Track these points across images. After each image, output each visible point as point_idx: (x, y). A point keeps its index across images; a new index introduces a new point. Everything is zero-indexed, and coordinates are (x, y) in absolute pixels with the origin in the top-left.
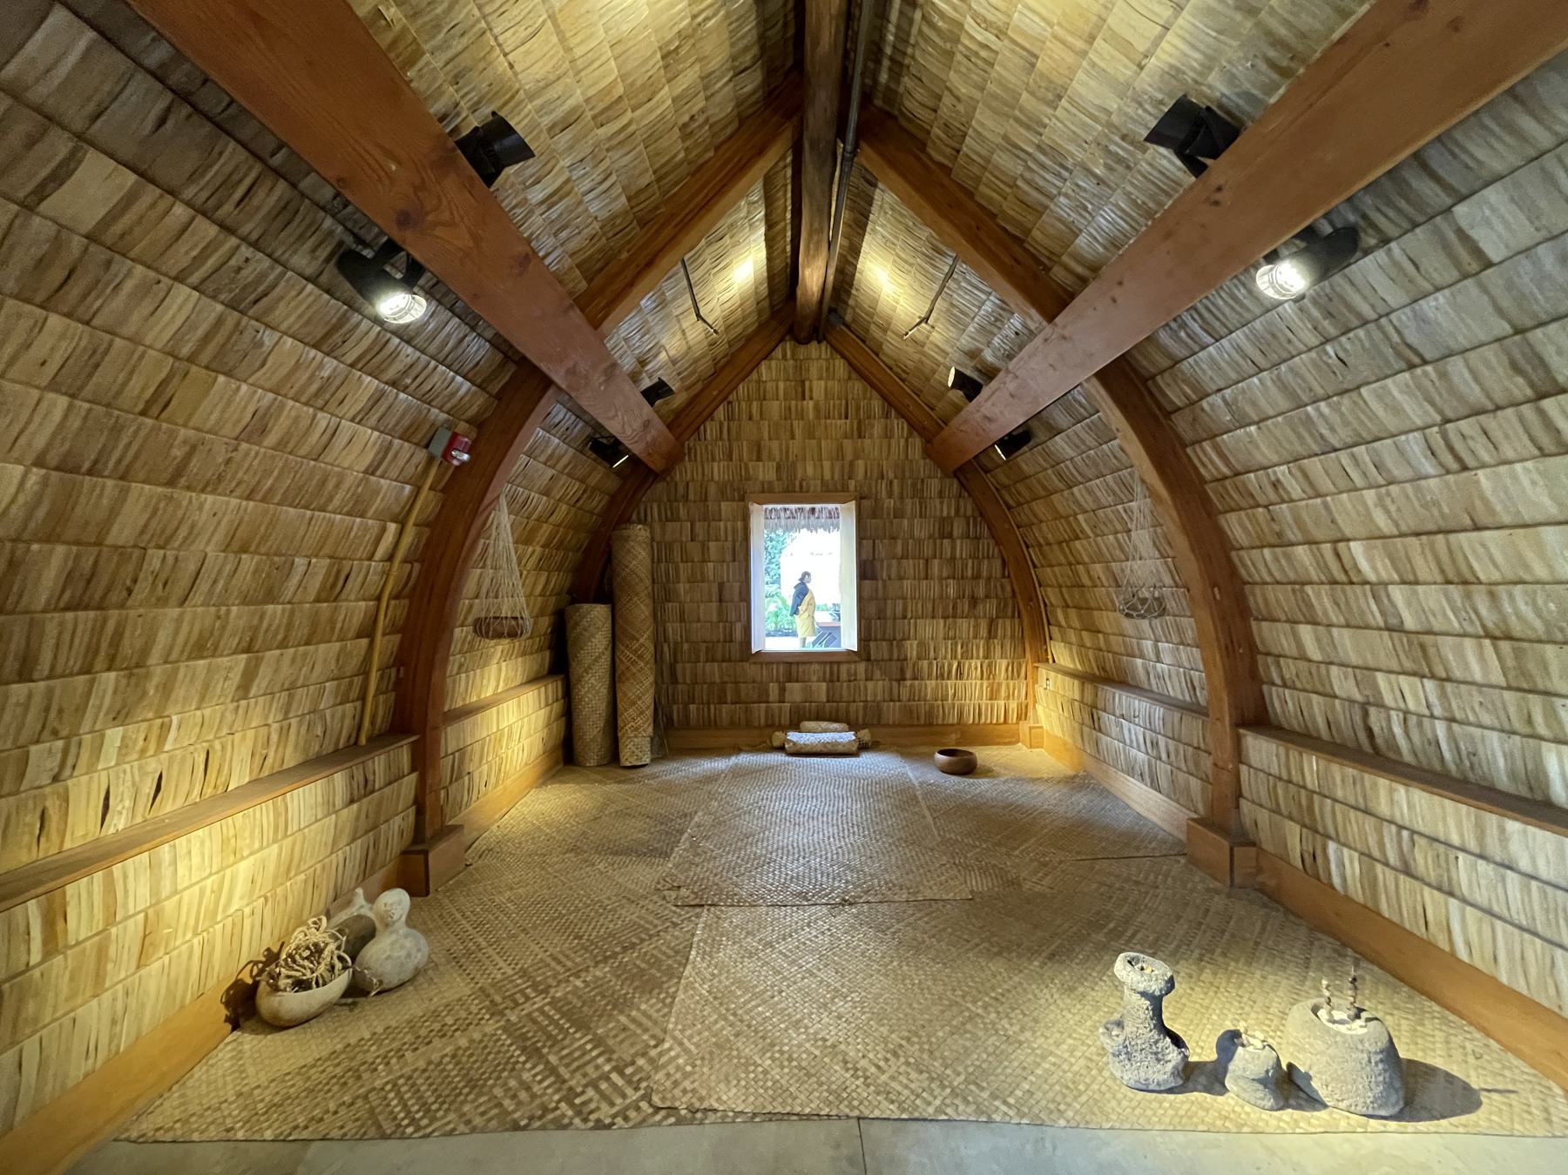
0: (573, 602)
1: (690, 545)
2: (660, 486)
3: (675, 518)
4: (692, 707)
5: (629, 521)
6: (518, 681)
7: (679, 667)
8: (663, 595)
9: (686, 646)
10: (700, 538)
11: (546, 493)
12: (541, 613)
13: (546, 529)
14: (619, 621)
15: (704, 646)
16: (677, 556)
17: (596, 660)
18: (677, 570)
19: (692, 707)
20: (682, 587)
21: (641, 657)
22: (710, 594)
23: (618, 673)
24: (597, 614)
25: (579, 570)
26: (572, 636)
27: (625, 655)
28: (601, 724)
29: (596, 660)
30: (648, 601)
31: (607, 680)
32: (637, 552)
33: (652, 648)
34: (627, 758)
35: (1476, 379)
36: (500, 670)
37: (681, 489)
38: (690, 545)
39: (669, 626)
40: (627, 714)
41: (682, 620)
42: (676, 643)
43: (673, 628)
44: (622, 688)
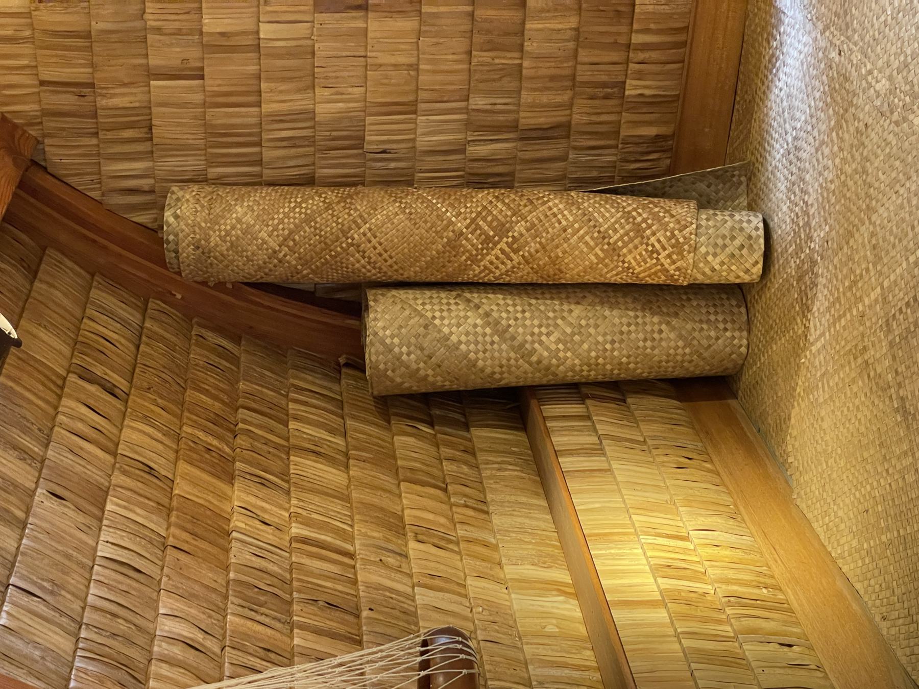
0: (357, 364)
1: (212, 83)
2: (62, 155)
3: (143, 123)
4: (632, 89)
5: (155, 232)
6: (542, 521)
7: (527, 119)
8: (348, 163)
9: (478, 102)
10: (193, 54)
11: (94, 499)
12: (386, 459)
13: (190, 483)
14: (410, 274)
15: (479, 57)
16: (246, 116)
17: (502, 333)
18: (280, 118)
19: (632, 89)
20: (327, 107)
21: (502, 229)
22: (351, 34)
23: (534, 278)
24: (394, 329)
25: (276, 349)
26: (441, 382)
27: (496, 262)
28: (653, 321)
29: (502, 333)
30: (361, 206)
31: (549, 307)
32: (234, 225)
33: (483, 197)
34: (747, 268)
35: (149, 499)
36: (526, 584)
37: (66, 101)
38: (212, 83)
39: (424, 141)
40: (638, 265)
41: (411, 108)
42: (468, 125)
43: (432, 130)
44: (574, 272)
